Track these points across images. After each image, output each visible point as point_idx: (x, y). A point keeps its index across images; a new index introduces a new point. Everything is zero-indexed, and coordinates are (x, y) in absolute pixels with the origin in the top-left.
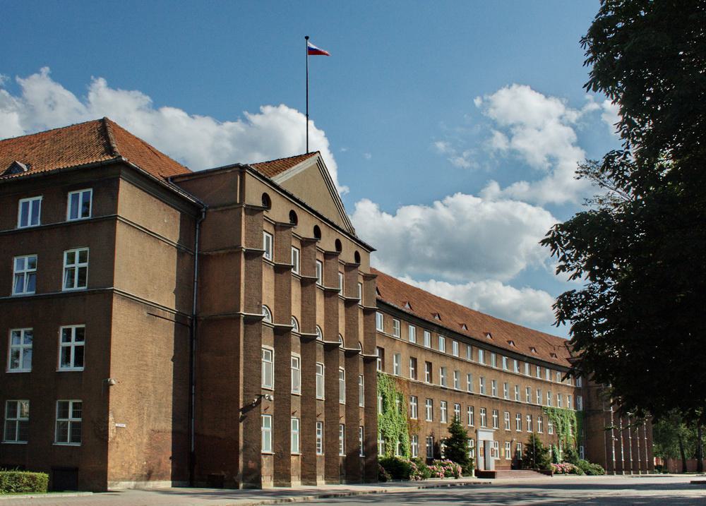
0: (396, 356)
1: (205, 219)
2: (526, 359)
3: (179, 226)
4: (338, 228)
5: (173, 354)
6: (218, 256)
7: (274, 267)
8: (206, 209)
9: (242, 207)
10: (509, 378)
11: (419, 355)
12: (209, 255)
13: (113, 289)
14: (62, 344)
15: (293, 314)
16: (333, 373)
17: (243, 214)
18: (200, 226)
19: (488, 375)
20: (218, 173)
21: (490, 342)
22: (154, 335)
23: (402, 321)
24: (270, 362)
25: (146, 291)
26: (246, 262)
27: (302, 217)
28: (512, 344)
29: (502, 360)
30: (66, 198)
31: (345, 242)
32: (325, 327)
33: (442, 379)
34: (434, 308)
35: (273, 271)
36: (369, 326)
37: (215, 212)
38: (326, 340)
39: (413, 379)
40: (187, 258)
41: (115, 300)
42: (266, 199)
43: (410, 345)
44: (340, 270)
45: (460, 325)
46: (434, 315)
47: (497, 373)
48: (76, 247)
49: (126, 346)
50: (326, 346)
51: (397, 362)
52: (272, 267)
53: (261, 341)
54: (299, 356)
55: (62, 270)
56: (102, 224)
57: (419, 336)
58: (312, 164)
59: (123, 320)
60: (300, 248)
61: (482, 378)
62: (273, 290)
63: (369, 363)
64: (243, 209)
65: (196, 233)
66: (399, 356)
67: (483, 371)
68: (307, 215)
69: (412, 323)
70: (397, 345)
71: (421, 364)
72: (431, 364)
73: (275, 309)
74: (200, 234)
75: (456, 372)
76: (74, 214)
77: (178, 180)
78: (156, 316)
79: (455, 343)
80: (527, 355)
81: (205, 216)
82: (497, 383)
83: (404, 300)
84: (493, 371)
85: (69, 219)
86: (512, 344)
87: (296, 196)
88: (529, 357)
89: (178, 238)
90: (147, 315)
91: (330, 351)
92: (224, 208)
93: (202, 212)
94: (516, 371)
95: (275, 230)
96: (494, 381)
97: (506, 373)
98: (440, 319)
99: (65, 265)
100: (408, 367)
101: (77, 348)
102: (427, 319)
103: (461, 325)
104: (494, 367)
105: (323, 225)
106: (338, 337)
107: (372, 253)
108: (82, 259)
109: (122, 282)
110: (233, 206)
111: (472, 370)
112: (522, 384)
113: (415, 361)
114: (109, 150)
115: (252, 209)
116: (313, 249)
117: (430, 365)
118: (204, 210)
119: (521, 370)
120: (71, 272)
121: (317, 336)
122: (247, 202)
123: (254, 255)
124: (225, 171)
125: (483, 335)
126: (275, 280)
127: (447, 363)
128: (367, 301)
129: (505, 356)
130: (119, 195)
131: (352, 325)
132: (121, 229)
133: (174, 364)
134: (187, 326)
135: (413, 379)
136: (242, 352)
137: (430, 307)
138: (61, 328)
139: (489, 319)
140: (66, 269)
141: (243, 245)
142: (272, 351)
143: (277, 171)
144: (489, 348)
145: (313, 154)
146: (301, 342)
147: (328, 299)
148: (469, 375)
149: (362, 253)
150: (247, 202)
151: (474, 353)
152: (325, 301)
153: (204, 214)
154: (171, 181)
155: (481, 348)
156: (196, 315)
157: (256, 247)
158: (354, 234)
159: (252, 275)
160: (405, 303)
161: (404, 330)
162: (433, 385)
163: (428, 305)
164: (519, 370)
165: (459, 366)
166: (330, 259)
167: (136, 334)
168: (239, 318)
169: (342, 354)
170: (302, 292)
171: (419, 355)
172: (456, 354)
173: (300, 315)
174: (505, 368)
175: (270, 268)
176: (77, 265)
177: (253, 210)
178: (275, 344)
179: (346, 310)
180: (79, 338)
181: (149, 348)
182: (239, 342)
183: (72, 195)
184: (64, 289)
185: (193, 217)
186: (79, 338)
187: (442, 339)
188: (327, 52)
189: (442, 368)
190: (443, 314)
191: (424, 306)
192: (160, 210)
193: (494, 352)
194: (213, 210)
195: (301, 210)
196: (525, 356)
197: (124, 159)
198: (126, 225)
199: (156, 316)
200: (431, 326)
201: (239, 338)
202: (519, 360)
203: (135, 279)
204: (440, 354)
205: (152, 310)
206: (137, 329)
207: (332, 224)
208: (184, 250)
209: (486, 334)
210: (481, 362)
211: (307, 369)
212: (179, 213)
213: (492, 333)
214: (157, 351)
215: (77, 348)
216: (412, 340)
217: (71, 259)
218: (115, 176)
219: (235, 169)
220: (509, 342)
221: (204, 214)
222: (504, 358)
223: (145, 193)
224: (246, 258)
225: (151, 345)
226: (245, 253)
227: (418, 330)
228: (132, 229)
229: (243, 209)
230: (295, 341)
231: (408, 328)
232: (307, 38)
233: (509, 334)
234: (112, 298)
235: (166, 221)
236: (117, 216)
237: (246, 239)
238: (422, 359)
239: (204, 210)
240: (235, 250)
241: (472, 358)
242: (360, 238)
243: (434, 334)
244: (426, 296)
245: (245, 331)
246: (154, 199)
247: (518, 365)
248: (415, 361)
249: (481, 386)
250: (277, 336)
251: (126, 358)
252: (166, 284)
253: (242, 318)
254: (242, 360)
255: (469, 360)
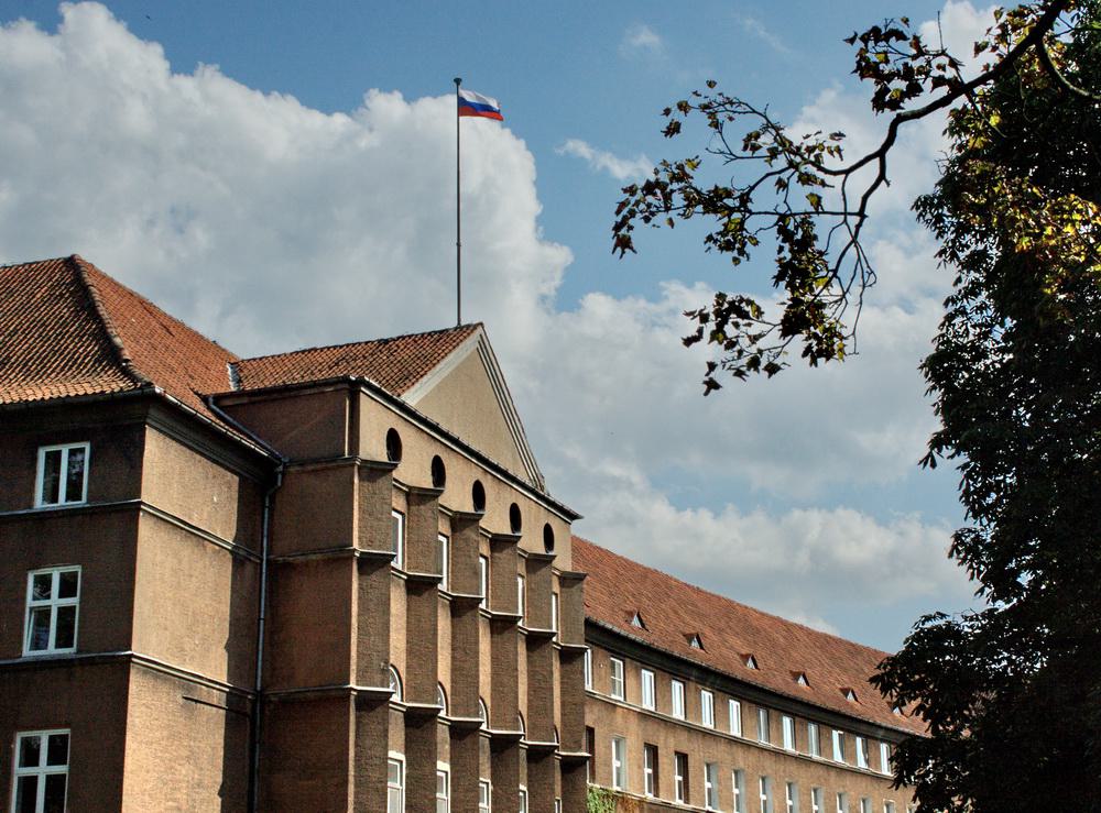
0: (617, 743)
1: (279, 488)
2: (881, 733)
3: (236, 506)
4: (514, 479)
5: (220, 780)
6: (306, 564)
7: (406, 580)
8: (285, 467)
9: (353, 465)
10: (849, 780)
11: (662, 738)
12: (289, 564)
13: (132, 655)
14: (19, 771)
15: (391, 662)
16: (508, 799)
17: (356, 480)
18: (272, 501)
19: (804, 777)
20: (308, 392)
21: (805, 698)
22: (192, 743)
23: (628, 660)
24: (398, 785)
25: (183, 650)
26: (359, 579)
27: (456, 468)
28: (850, 697)
29: (830, 739)
30: (34, 460)
31: (528, 508)
32: (492, 699)
33: (709, 790)
34: (688, 619)
35: (403, 589)
36: (572, 685)
37: (303, 472)
38: (454, 714)
39: (650, 797)
40: (249, 568)
41: (133, 672)
42: (393, 440)
43: (644, 716)
44: (519, 571)
45: (742, 656)
46: (689, 638)
47: (821, 771)
48: (54, 564)
49: (148, 772)
50: (494, 739)
51: (618, 758)
52: (402, 582)
53: (387, 745)
54: (402, 757)
55: (24, 610)
56: (114, 516)
57: (662, 695)
58: (469, 352)
59: (146, 709)
60: (449, 534)
61: (790, 785)
62: (405, 631)
63: (419, 727)
64: (356, 468)
65: (263, 518)
66: (622, 744)
67: (793, 767)
68: (461, 461)
69: (647, 665)
70: (619, 716)
71: (665, 760)
72: (819, 198)
73: (408, 673)
74: (271, 516)
75: (736, 772)
76: (52, 495)
77: (228, 402)
78: (197, 701)
79: (734, 705)
80: (884, 724)
81: (282, 482)
82: (821, 794)
83: (629, 608)
84: (813, 766)
85: (39, 504)
86: (850, 697)
87: (444, 427)
88: (887, 729)
89: (234, 532)
90: (181, 701)
91: (502, 751)
92: (319, 466)
93: (277, 474)
94: (862, 764)
95: (409, 504)
96: (815, 791)
97: (762, 749)
98: (702, 648)
99: (30, 602)
100: (640, 767)
101: (49, 778)
102: (676, 654)
103: (745, 657)
104: (815, 756)
105: (489, 477)
106: (436, 690)
107: (575, 522)
108: (67, 588)
109: (147, 641)
110: (337, 461)
111: (769, 765)
112: (876, 794)
113: (653, 751)
114: (111, 356)
115: (371, 469)
116: (473, 536)
117: (683, 758)
118: (281, 468)
119: (872, 761)
120: (42, 616)
121: (391, 694)
122: (363, 454)
123: (375, 564)
124: (321, 389)
125: (789, 679)
126: (408, 610)
127: (720, 752)
128: (567, 633)
129: (837, 728)
130: (145, 459)
131: (539, 689)
132: (146, 529)
133: (222, 802)
134: (245, 714)
135: (650, 797)
136: (352, 772)
137: (679, 617)
138: (19, 737)
139: (799, 634)
140: (32, 609)
141: (356, 545)
142: (401, 762)
143: (410, 377)
144: (803, 711)
145: (472, 328)
146: (451, 738)
147: (498, 638)
148: (763, 779)
149: (556, 525)
150: (363, 454)
151: (773, 725)
152: (492, 642)
153: (280, 476)
154: (215, 404)
155: (788, 713)
156: (261, 691)
157: (380, 547)
158: (542, 488)
159: (372, 606)
160: (631, 614)
161: (631, 682)
162: (690, 807)
163: (676, 612)
164: (867, 761)
165: (743, 759)
166: (501, 551)
167: (164, 743)
168: (349, 696)
169: (485, 742)
170: (453, 626)
171: (662, 738)
172: (735, 731)
173: (449, 678)
174: (838, 758)
175: (399, 585)
176: (55, 602)
177: (375, 471)
178: (406, 747)
179: (528, 656)
180: (54, 759)
181: (184, 772)
182: (348, 749)
183: (47, 453)
184: (27, 652)
185: (260, 488)
186: (54, 759)
187: (706, 696)
188: (494, 104)
189: (708, 766)
190: (707, 631)
191: (667, 618)
192: (207, 478)
193: (814, 721)
194: (298, 468)
195: (452, 454)
196: (880, 727)
197: (158, 391)
198: (170, 526)
199: (197, 701)
200: (683, 669)
201: (347, 741)
202: (867, 737)
203: (166, 629)
204: (705, 733)
205: (187, 685)
206: (165, 733)
207: (505, 473)
208: (242, 557)
209: (796, 676)
210: (788, 746)
211: (461, 796)
212: (237, 478)
213: (809, 672)
214: (196, 776)
215: (49, 778)
216: (648, 704)
217: (44, 584)
218: (138, 421)
219: (340, 386)
220: (845, 692)
221: (280, 476)
222: (836, 734)
223: (184, 448)
224: (361, 572)
225: (187, 766)
226: (358, 559)
227: (659, 678)
228: (160, 523)
229: (356, 468)
230: (443, 733)
231: (639, 676)
232: (458, 81)
233: (845, 670)
234: (129, 673)
235: (215, 499)
236: (141, 503)
237: (360, 531)
238: (668, 745)
239: (281, 468)
240: (339, 555)
241: (768, 738)
242: (553, 498)
243: (692, 685)
244: (669, 587)
245: (358, 723)
246: (198, 457)
247: (866, 750)
248: (653, 751)
249: (763, 797)
250: (411, 730)
251: (147, 798)
252: (214, 630)
253: (352, 698)
254: (351, 788)
255: (763, 742)
